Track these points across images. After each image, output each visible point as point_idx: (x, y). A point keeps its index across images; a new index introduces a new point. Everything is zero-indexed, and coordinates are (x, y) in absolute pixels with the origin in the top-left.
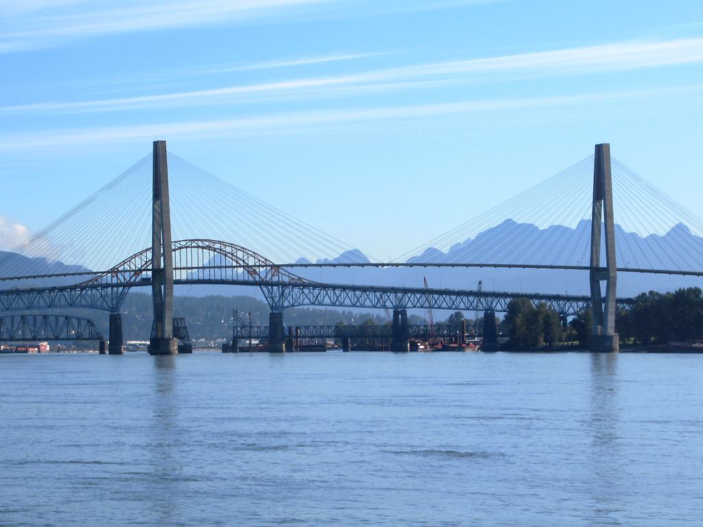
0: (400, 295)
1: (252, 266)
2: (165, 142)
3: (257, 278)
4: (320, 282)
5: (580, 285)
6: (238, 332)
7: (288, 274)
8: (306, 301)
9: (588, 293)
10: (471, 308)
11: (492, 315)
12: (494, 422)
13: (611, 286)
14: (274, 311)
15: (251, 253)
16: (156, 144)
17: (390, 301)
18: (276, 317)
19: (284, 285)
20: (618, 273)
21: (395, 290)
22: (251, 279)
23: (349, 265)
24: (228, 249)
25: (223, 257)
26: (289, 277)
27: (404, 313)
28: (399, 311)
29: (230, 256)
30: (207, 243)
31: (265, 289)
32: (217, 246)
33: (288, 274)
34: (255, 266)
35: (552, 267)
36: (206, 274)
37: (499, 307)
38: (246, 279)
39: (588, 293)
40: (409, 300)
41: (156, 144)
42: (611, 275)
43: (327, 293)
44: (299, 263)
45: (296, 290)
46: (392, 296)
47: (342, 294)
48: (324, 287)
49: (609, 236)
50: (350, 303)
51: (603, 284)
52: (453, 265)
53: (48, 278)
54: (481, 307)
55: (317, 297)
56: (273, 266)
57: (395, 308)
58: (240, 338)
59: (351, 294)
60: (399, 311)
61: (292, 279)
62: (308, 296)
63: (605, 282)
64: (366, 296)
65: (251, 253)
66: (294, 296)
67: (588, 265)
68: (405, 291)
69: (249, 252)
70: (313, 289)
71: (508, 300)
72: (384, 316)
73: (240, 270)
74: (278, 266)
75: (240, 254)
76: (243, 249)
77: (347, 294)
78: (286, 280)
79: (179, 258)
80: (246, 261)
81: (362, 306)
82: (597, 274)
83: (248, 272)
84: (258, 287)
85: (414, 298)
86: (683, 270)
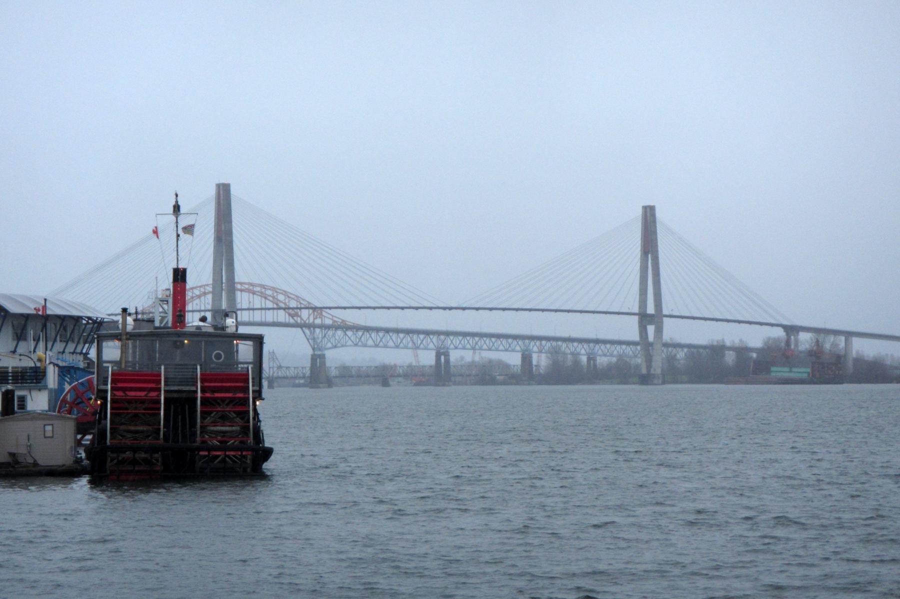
0: (442, 337)
1: (293, 309)
2: (643, 207)
3: (299, 320)
5: (629, 329)
6: (274, 373)
7: (331, 317)
8: (350, 343)
9: (636, 337)
10: (339, 345)
13: (659, 331)
14: (316, 353)
16: (645, 208)
17: (518, 345)
18: (317, 360)
19: (328, 327)
20: (665, 319)
21: (438, 333)
22: (292, 321)
23: (417, 308)
24: (269, 292)
25: (251, 295)
26: (332, 319)
27: (595, 360)
28: (442, 353)
29: (271, 299)
30: (247, 286)
31: (307, 331)
32: (258, 289)
33: (331, 317)
34: (297, 308)
36: (76, 306)
37: (583, 352)
38: (287, 321)
39: (636, 337)
40: (449, 341)
41: (645, 208)
43: (600, 348)
45: (339, 333)
46: (435, 339)
47: (579, 346)
48: (367, 329)
50: (394, 345)
51: (651, 329)
52: (530, 310)
54: (431, 346)
55: (361, 338)
56: (315, 309)
59: (394, 336)
60: (442, 353)
62: (352, 338)
64: (581, 346)
66: (337, 338)
67: (636, 310)
69: (278, 291)
71: (686, 350)
72: (427, 358)
73: (281, 312)
75: (281, 297)
76: (285, 293)
77: (518, 342)
78: (328, 322)
79: (243, 299)
80: (288, 304)
81: (497, 350)
82: (644, 319)
83: (290, 315)
84: (299, 330)
85: (457, 341)
86: (706, 316)
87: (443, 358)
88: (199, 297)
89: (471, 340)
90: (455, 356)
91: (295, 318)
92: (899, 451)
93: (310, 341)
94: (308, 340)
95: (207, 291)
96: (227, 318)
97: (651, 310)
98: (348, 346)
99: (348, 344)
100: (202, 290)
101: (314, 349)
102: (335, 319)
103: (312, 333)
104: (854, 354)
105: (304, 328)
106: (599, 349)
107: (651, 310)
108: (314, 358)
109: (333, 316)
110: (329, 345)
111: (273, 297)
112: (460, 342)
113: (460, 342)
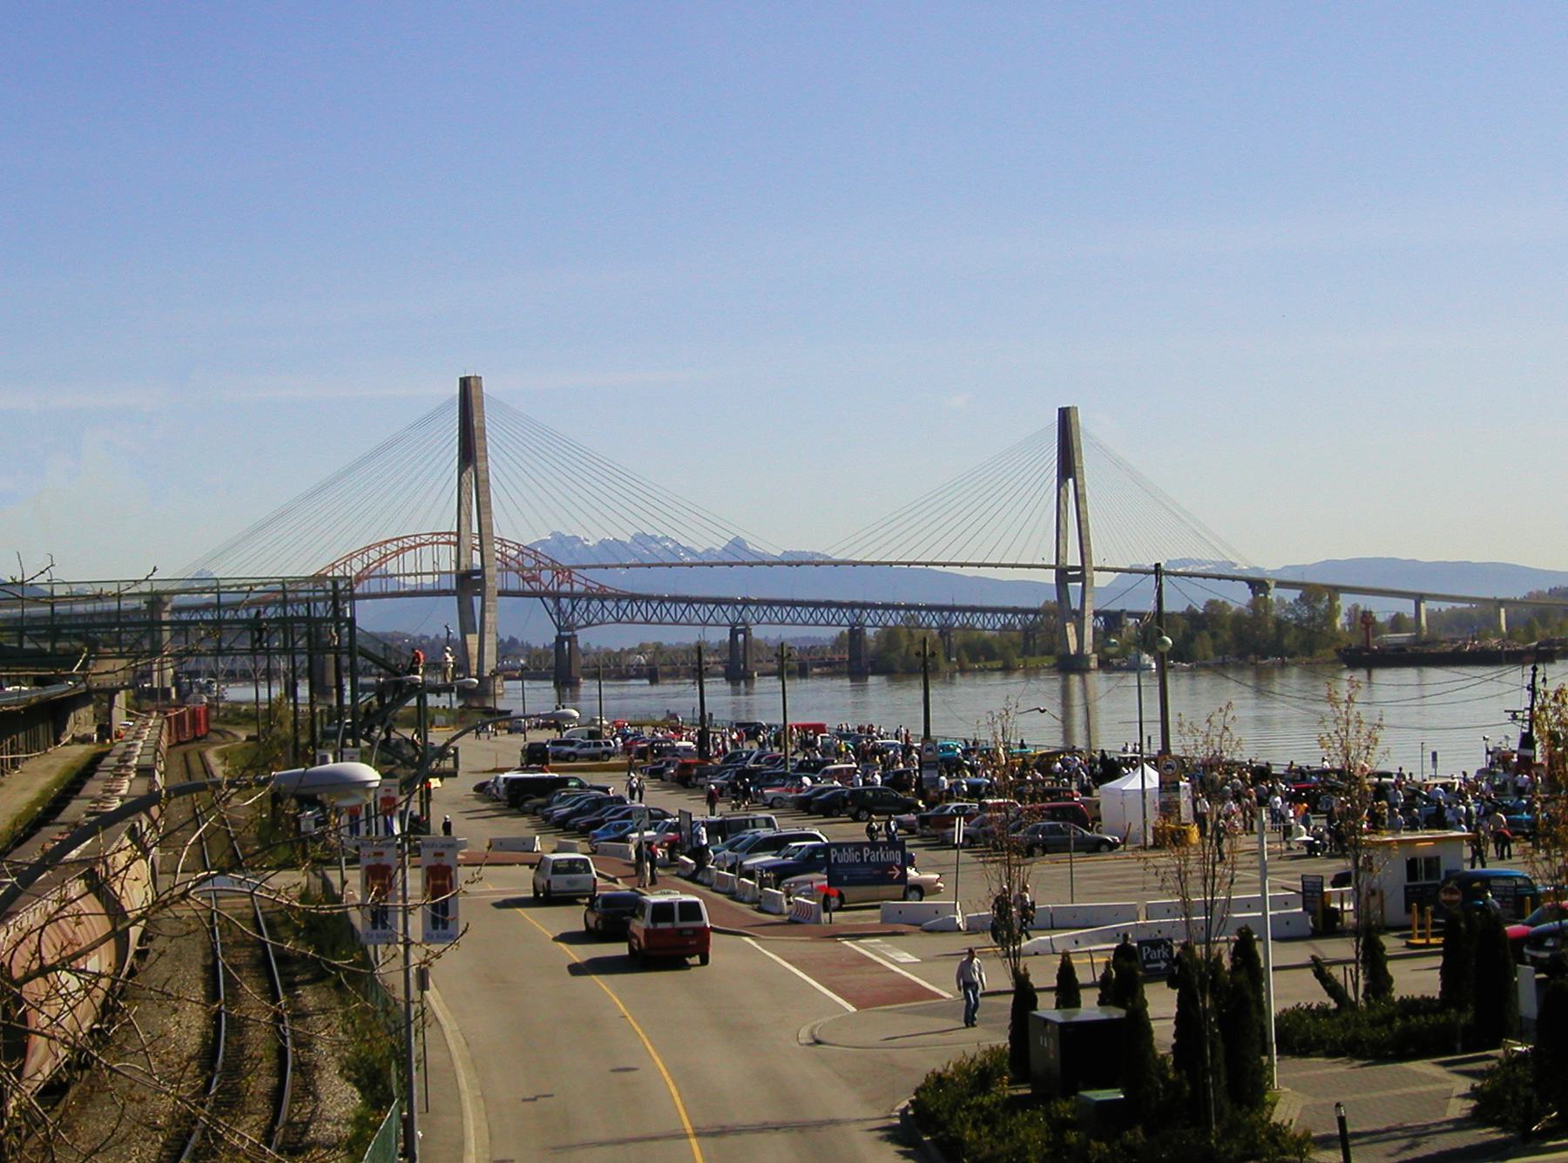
4: (630, 591)
7: (584, 582)
11: (861, 632)
12: (101, 677)
14: (562, 633)
15: (512, 545)
22: (527, 588)
33: (584, 582)
35: (1029, 566)
40: (750, 614)
42: (1088, 575)
44: (786, 560)
49: (1083, 526)
53: (813, 566)
54: (725, 621)
57: (852, 625)
58: (269, 658)
61: (590, 588)
63: (480, 598)
65: (512, 545)
68: (864, 606)
69: (507, 544)
70: (298, 605)
72: (826, 634)
74: (569, 569)
87: (741, 637)
88: (397, 554)
89: (644, 604)
90: (758, 633)
91: (533, 583)
92: (1563, 913)
93: (554, 616)
94: (551, 615)
95: (406, 545)
96: (1248, 612)
97: (1073, 559)
98: (666, 624)
99: (636, 619)
100: (400, 544)
101: (559, 628)
102: (589, 584)
103: (557, 603)
104: (202, 974)
105: (545, 599)
106: (868, 618)
107: (1073, 559)
108: (560, 640)
109: (586, 580)
110: (582, 622)
111: (502, 553)
112: (811, 615)
113: (811, 615)
